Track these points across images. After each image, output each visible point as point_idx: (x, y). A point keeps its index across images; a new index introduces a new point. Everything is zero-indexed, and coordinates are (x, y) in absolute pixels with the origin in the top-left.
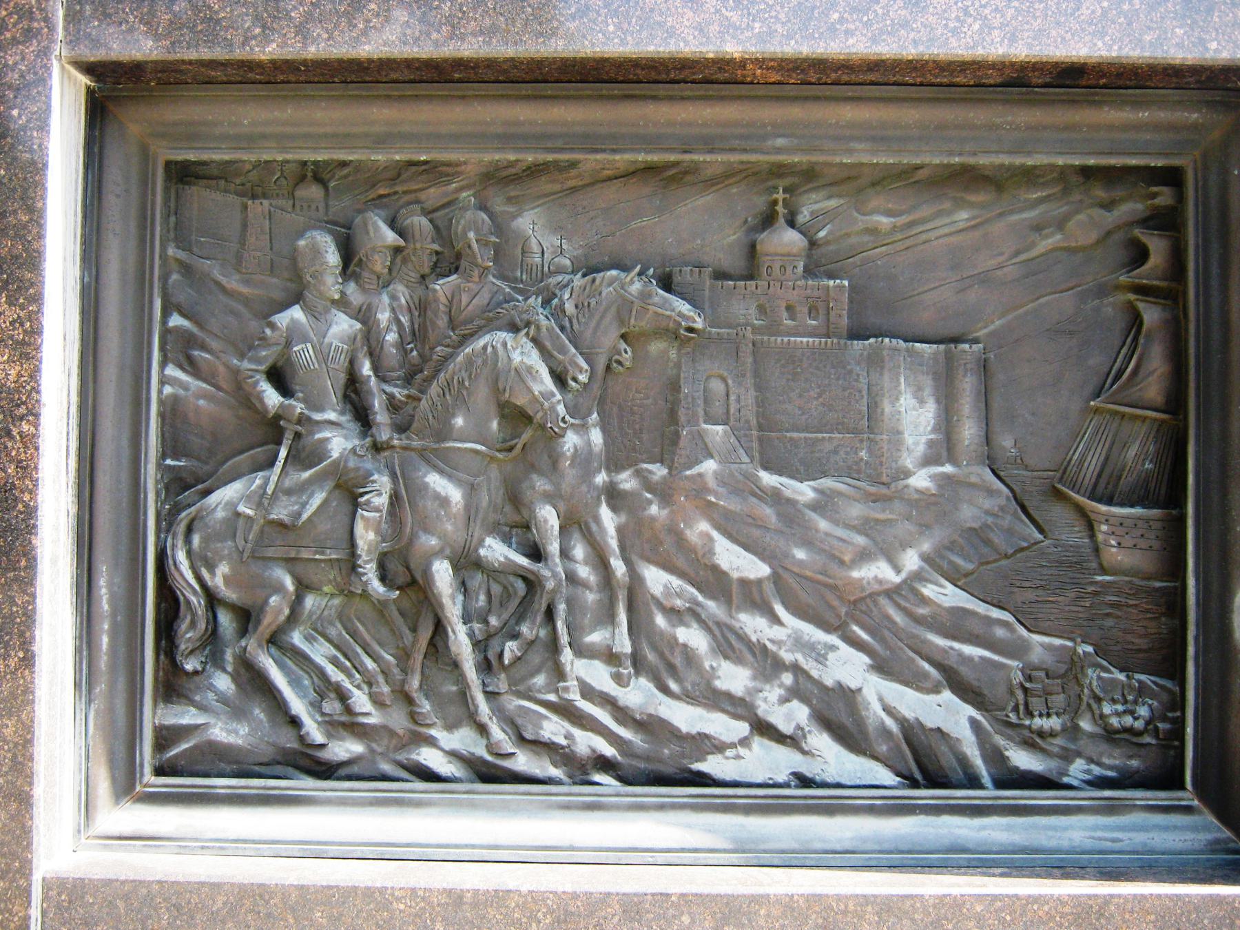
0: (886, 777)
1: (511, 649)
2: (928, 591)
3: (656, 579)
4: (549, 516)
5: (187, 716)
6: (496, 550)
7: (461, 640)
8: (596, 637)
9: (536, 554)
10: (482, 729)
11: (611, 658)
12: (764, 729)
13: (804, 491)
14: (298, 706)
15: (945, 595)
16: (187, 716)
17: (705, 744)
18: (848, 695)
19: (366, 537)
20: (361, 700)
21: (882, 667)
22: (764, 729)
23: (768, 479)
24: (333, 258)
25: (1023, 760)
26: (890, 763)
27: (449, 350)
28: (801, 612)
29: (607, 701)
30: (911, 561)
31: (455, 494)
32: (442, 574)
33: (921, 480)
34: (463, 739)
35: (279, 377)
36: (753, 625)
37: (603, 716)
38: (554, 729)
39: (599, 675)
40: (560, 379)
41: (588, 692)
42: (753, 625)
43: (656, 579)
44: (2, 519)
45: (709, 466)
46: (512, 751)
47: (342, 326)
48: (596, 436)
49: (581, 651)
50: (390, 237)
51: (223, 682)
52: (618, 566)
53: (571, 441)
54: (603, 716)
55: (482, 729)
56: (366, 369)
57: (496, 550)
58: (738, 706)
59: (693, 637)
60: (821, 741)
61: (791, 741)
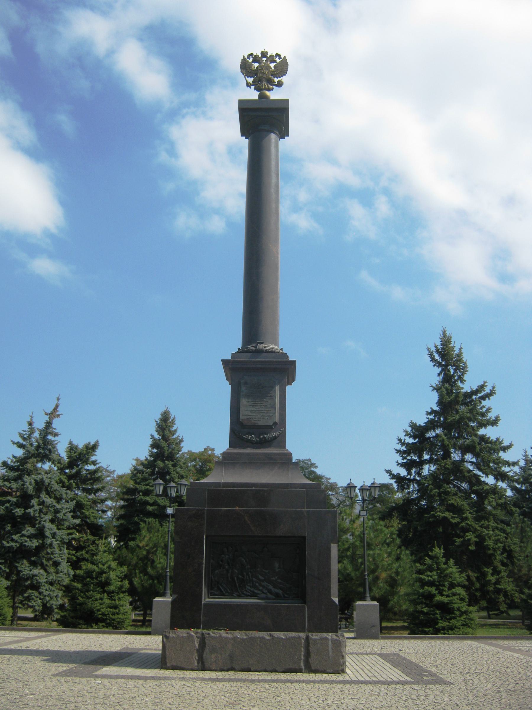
0: (274, 597)
1: (241, 585)
2: (278, 580)
3: (254, 579)
4: (245, 574)
5: (213, 591)
6: (240, 576)
7: (237, 584)
8: (249, 584)
9: (244, 577)
10: (239, 592)
11: (250, 586)
12: (263, 593)
13: (267, 571)
14: (223, 590)
15: (279, 581)
16: (213, 591)
17: (258, 594)
18: (271, 590)
19: (229, 575)
20: (228, 590)
21: (274, 587)
22: (263, 593)
23: (264, 570)
24: (226, 550)
25: (286, 596)
26: (225, 668)
27: (282, 596)
28: (266, 582)
29: (250, 590)
30: (276, 578)
31: (237, 571)
32: (236, 578)
33: (277, 570)
34: (237, 593)
35: (222, 561)
36: (263, 583)
37: (249, 591)
38: (245, 592)
39: (249, 588)
40: (246, 561)
41: (248, 589)
42: (263, 583)
43: (254, 579)
44: (1, 503)
45: (259, 569)
46: (49, 536)
47: (227, 556)
48: (249, 566)
49: (247, 586)
50: (231, 548)
51: (216, 589)
52: (251, 578)
53: (247, 567)
54: (249, 591)
55: (239, 592)
56: (229, 560)
57: (240, 576)
58: (261, 591)
59: (257, 584)
60: (268, 594)
61: (266, 594)
